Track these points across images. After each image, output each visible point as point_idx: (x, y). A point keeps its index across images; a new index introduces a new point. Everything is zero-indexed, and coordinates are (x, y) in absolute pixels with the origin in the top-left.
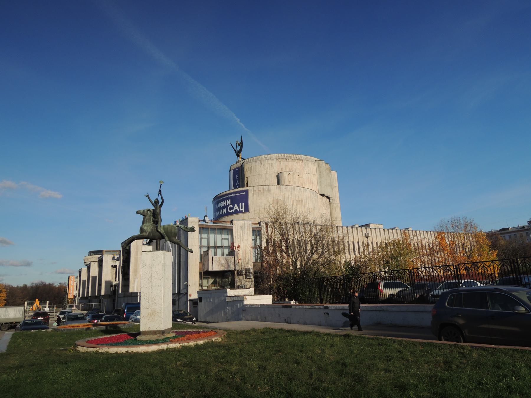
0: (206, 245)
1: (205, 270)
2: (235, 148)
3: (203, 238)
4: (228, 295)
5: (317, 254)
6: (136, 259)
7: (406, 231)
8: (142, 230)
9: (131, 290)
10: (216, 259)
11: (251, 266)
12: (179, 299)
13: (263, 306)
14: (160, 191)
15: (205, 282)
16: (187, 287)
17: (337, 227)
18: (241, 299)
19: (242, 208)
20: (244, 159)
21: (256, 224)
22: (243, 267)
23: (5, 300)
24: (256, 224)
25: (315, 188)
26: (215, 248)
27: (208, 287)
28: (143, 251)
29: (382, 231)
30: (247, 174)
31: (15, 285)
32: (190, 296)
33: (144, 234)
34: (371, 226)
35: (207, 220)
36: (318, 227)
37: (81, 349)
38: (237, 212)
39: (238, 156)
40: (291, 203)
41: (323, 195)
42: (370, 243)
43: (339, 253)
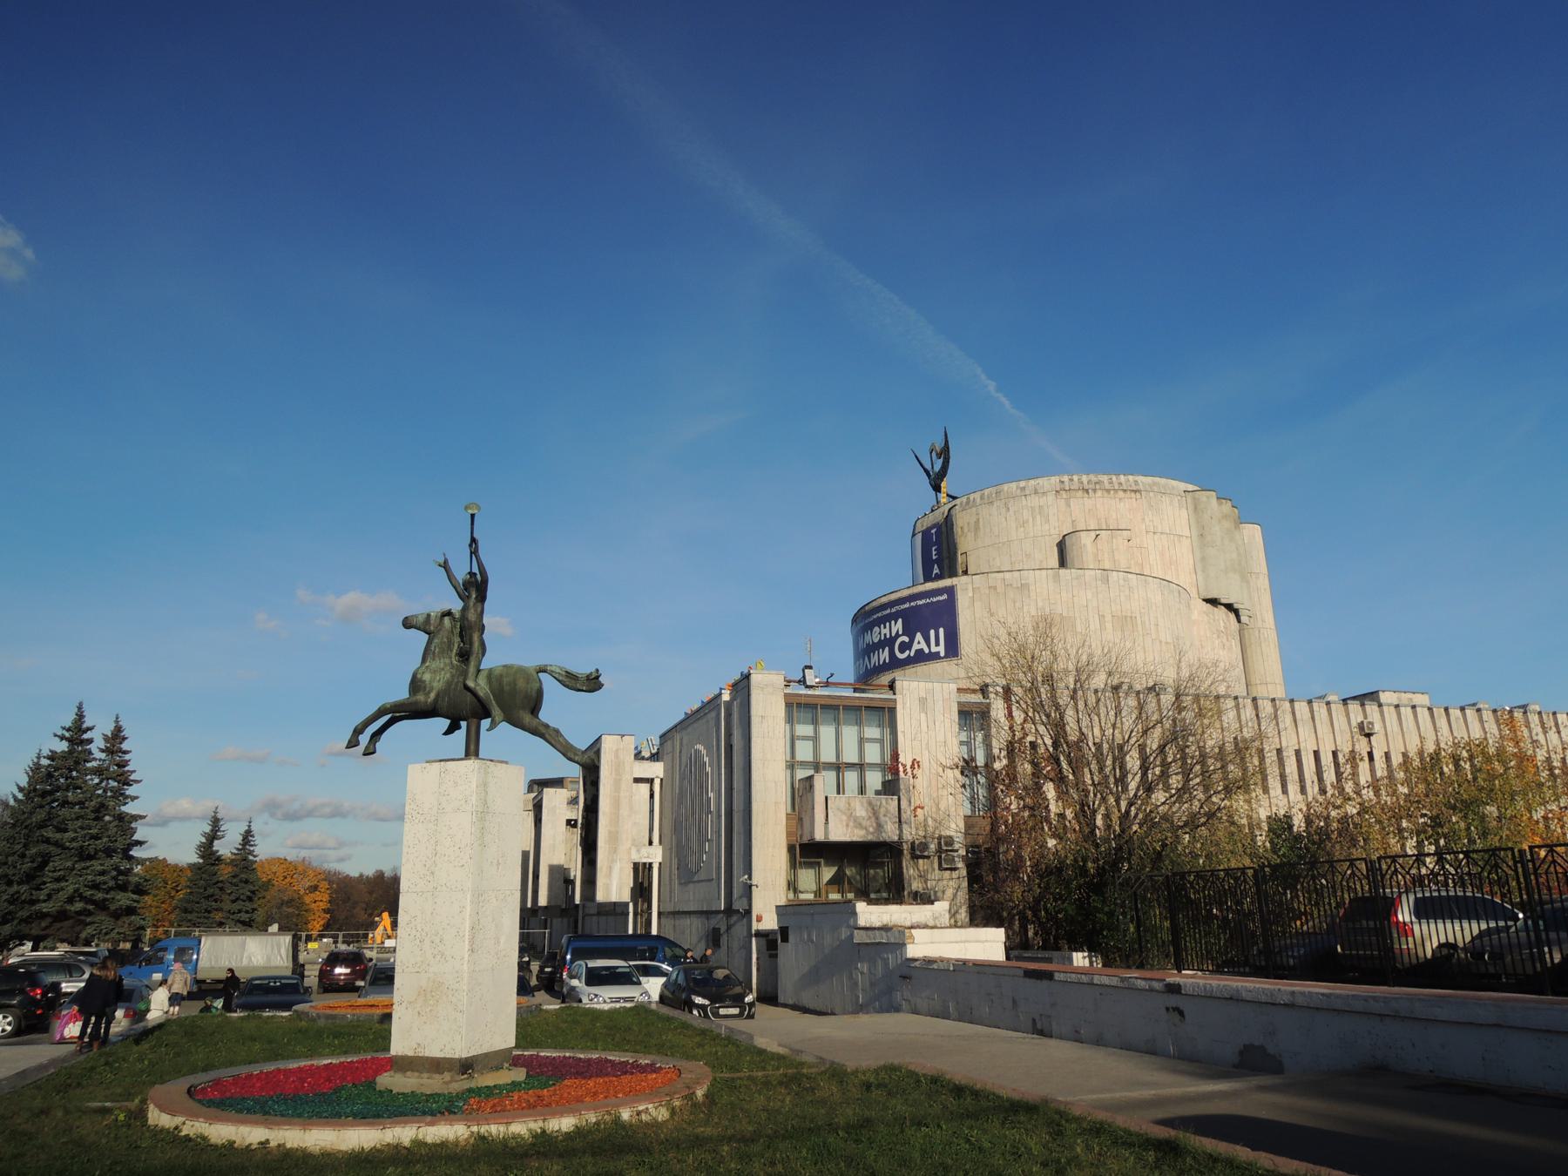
0: (833, 760)
1: (805, 840)
2: (928, 467)
4: (862, 922)
5: (1167, 788)
6: (617, 803)
7: (1518, 715)
8: (416, 685)
10: (837, 802)
11: (954, 828)
12: (729, 928)
13: (964, 966)
14: (473, 540)
15: (807, 878)
16: (748, 889)
18: (893, 939)
19: (937, 644)
20: (954, 498)
21: (974, 691)
22: (930, 829)
23: (326, 911)
24: (974, 691)
25: (1186, 579)
26: (839, 767)
27: (818, 893)
29: (1423, 714)
30: (965, 542)
31: (355, 874)
32: (759, 919)
33: (420, 697)
34: (1383, 697)
35: (811, 678)
36: (1167, 699)
37: (158, 1118)
38: (921, 657)
39: (937, 489)
40: (1094, 624)
41: (1213, 602)
42: (1377, 755)
43: (1242, 785)
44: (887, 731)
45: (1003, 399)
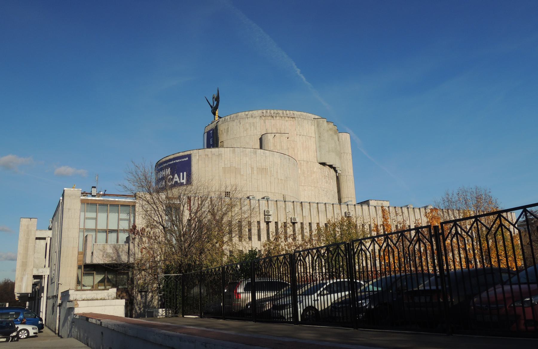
2: (212, 104)
3: (122, 220)
9: (123, 302)
17: (301, 203)
19: (183, 179)
28: (37, 238)
30: (222, 137)
34: (372, 203)
41: (323, 164)
44: (132, 215)
45: (303, 77)
